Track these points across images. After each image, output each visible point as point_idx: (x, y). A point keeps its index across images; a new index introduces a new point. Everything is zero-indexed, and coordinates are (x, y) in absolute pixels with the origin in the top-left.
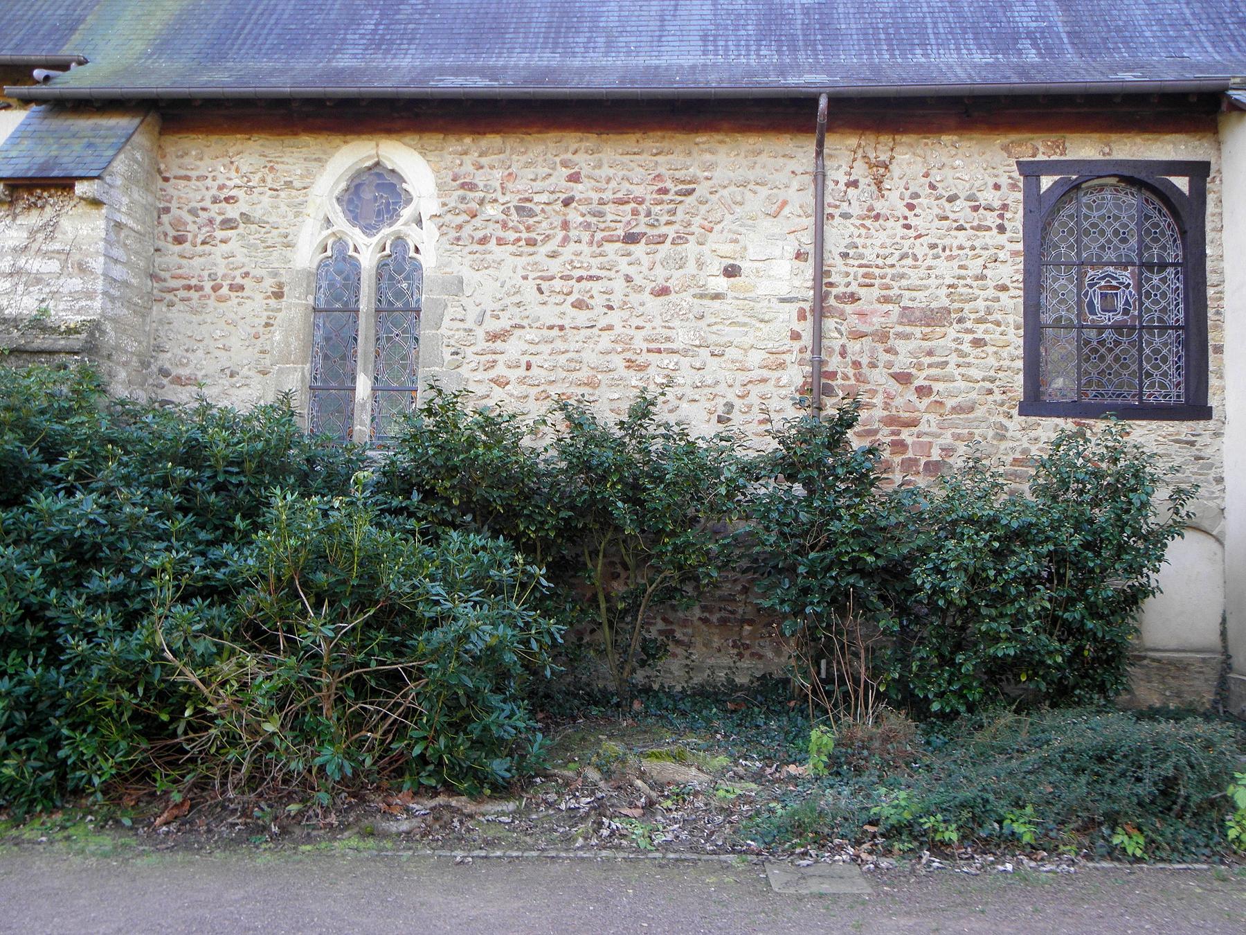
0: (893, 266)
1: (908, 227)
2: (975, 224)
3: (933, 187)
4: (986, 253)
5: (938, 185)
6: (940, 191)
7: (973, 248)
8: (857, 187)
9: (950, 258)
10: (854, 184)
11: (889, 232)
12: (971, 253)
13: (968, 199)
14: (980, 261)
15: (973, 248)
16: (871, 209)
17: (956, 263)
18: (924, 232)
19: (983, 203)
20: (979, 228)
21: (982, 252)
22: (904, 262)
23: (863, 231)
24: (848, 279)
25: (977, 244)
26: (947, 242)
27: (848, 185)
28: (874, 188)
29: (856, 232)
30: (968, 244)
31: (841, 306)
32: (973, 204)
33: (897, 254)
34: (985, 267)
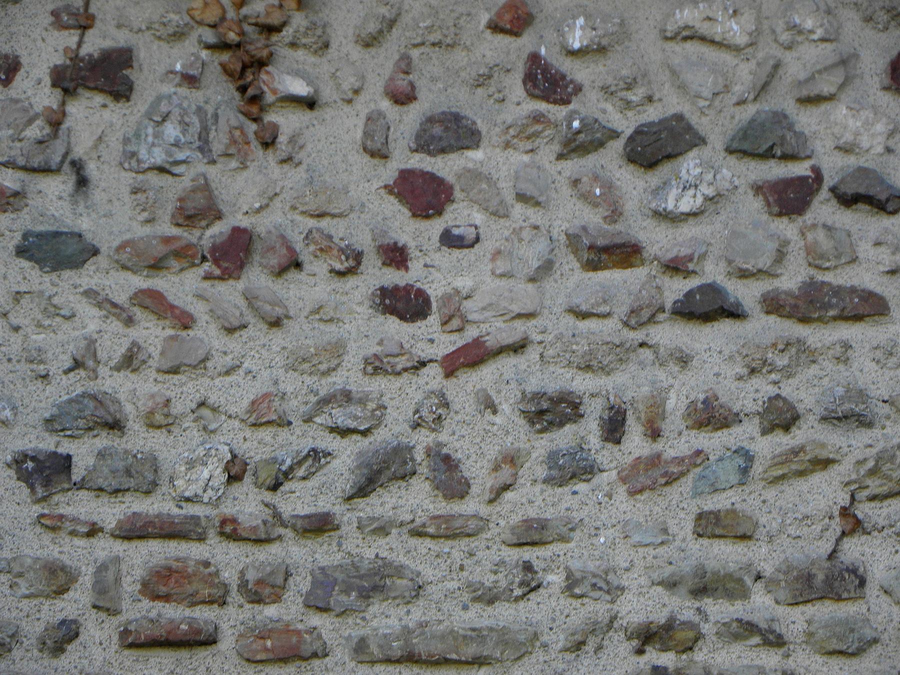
0: (319, 526)
1: (406, 304)
2: (791, 279)
3: (546, 82)
4: (855, 445)
5: (579, 72)
6: (592, 105)
7: (781, 417)
8: (121, 91)
9: (652, 476)
10: (109, 75)
11: (302, 334)
12: (767, 447)
13: (749, 145)
14: (824, 492)
15: (781, 417)
16: (198, 210)
17: (680, 505)
18: (499, 332)
19: (834, 166)
20: (809, 305)
21: (834, 439)
22: (385, 503)
23: (152, 333)
24: (55, 610)
25: (804, 391)
26: (631, 383)
27: (70, 79)
28: (218, 93)
29: (114, 341)
30: (750, 395)
31: (434, 305)
32: (776, 171)
33: (346, 456)
34: (853, 524)
